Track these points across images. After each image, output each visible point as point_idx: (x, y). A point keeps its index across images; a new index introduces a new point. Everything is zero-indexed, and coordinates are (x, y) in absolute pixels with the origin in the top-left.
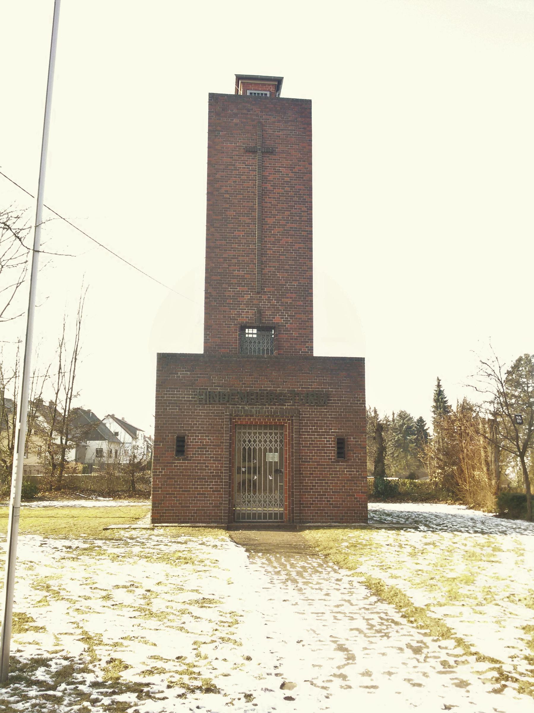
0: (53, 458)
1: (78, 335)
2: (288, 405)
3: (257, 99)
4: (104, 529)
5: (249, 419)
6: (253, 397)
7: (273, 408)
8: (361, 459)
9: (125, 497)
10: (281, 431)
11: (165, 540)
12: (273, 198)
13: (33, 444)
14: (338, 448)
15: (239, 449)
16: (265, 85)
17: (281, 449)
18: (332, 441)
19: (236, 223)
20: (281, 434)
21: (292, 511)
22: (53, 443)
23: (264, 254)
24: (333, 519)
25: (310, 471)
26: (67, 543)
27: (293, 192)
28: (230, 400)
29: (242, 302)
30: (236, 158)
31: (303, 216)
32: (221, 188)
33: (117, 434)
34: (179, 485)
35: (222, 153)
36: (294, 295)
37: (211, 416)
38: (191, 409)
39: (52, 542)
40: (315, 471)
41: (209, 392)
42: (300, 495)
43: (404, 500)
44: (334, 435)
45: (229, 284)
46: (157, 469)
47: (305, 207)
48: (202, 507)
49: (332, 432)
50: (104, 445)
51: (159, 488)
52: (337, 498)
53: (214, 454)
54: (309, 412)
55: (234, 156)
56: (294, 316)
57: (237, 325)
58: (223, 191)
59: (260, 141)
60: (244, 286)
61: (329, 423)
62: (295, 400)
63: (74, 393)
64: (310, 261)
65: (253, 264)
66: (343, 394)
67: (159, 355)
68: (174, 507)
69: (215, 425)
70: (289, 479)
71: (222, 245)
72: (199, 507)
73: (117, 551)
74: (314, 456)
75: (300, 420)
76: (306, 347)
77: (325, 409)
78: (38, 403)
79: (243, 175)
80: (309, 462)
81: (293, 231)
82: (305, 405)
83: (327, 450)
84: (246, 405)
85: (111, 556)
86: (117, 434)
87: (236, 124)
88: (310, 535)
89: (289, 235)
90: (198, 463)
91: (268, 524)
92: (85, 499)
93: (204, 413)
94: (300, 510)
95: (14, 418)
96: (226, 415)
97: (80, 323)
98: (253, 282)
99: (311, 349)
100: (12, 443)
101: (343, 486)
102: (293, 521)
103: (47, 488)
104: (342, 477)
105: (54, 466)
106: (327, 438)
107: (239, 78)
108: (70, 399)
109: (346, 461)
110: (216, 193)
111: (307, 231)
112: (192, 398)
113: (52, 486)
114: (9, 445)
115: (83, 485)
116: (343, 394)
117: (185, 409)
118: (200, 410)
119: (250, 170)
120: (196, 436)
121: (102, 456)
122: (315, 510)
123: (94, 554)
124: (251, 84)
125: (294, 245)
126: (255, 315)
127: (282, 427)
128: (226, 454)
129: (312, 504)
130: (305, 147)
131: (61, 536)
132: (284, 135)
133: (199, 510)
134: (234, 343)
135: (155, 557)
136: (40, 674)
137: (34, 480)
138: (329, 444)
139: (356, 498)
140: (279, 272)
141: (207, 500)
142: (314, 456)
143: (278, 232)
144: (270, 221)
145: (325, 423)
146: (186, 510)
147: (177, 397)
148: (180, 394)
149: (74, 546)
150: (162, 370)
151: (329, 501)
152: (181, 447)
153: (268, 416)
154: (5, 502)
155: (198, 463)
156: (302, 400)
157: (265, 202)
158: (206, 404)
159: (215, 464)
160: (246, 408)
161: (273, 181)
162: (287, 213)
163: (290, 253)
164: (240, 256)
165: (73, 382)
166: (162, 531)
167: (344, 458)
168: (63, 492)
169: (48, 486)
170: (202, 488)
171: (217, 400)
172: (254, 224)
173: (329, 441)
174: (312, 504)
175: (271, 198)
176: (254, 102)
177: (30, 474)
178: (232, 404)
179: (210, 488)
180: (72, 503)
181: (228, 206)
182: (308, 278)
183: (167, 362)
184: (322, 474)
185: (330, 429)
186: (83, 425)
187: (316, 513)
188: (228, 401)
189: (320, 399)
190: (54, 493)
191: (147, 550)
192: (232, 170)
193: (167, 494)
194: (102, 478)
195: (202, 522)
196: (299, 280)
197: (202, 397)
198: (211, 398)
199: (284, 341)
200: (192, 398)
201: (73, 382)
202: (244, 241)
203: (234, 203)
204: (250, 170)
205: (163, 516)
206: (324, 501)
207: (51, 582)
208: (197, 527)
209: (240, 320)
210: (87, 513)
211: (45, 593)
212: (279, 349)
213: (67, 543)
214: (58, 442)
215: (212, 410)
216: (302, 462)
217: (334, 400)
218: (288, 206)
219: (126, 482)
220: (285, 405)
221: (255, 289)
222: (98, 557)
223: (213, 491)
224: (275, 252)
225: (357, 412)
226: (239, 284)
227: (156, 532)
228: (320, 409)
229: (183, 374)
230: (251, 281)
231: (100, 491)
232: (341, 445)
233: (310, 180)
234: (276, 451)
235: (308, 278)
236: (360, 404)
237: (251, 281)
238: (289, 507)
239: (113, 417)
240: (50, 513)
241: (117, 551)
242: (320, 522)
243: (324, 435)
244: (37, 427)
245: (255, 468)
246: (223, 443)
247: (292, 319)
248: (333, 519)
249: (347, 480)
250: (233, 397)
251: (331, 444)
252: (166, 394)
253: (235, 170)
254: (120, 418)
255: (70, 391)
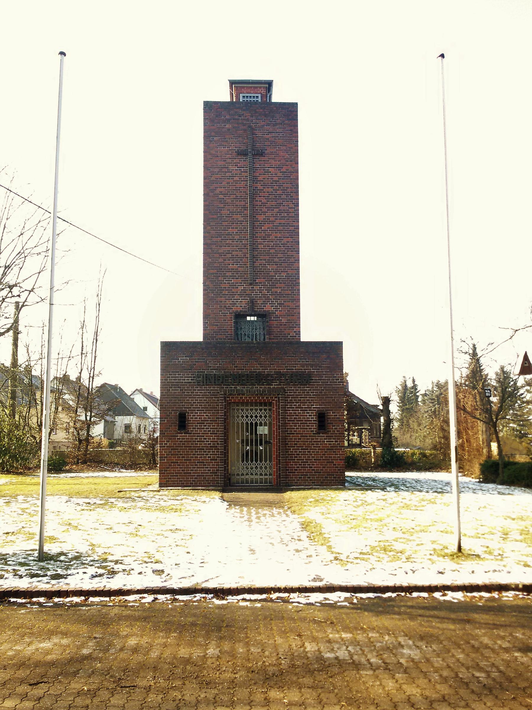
0: (78, 434)
1: (98, 317)
2: (275, 385)
3: (248, 105)
4: (118, 492)
5: (241, 398)
6: (243, 378)
7: (262, 388)
8: (339, 431)
9: (146, 469)
10: (270, 408)
11: (165, 498)
12: (263, 197)
13: (60, 420)
14: (319, 422)
15: (234, 423)
16: (256, 87)
17: (270, 423)
18: (314, 415)
19: (230, 221)
20: (270, 410)
21: (279, 476)
22: (79, 420)
23: (256, 249)
24: (315, 483)
25: (294, 441)
26: (87, 500)
27: (281, 190)
28: (224, 381)
29: (236, 292)
30: (229, 161)
31: (290, 212)
32: (216, 190)
33: (145, 409)
34: (182, 454)
35: (216, 157)
36: (283, 285)
37: (208, 395)
38: (190, 390)
39: (75, 500)
40: (298, 442)
41: (206, 374)
42: (286, 462)
43: (409, 469)
44: (315, 410)
45: (225, 277)
46: (163, 441)
47: (293, 204)
48: (202, 473)
49: (314, 408)
50: (132, 420)
51: (165, 457)
52: (318, 465)
53: (211, 428)
54: (293, 390)
55: (227, 159)
56: (283, 304)
57: (232, 313)
58: (218, 191)
59: (252, 146)
60: (238, 278)
61: (311, 400)
62: (281, 380)
63: (96, 372)
64: (297, 253)
65: (246, 258)
66: (324, 374)
67: (162, 343)
68: (178, 473)
69: (212, 403)
70: (277, 448)
71: (217, 242)
72: (199, 473)
73: (126, 505)
74: (298, 428)
75: (285, 398)
76: (294, 332)
77: (307, 387)
78: (65, 379)
79: (235, 177)
80: (294, 434)
81: (282, 226)
82: (289, 385)
83: (309, 423)
84: (238, 385)
85: (120, 508)
86: (145, 409)
87: (229, 130)
88: (288, 495)
89: (278, 230)
90: (197, 436)
91: (265, 487)
92: (109, 471)
93: (202, 393)
94: (286, 475)
95: (41, 397)
96: (221, 394)
97: (99, 305)
98: (246, 274)
99: (298, 333)
100: (41, 420)
101: (323, 454)
102: (280, 484)
103: (75, 461)
104: (322, 447)
105: (80, 441)
106: (309, 413)
107: (232, 83)
108: (93, 378)
109: (325, 433)
110: (211, 194)
111: (294, 226)
112: (191, 380)
113: (78, 460)
114: (38, 422)
115: (106, 458)
116: (324, 374)
117: (185, 390)
118: (198, 390)
119: (242, 172)
120: (195, 413)
121: (130, 432)
122: (299, 475)
123: (107, 507)
124: (244, 87)
125: (283, 240)
126: (248, 304)
127: (270, 404)
128: (221, 428)
129: (297, 470)
130: (292, 148)
131: (83, 496)
132: (272, 137)
133: (199, 476)
134: (230, 330)
135: (153, 509)
136: (62, 558)
137: (62, 454)
138: (311, 418)
139: (335, 465)
140: (269, 265)
141: (206, 468)
142: (298, 428)
143: (268, 228)
144: (261, 218)
145: (307, 400)
146: (188, 476)
147: (179, 380)
148: (181, 377)
149: (92, 503)
150: (165, 357)
151: (312, 467)
152: (182, 422)
153: (257, 395)
154: (36, 474)
155: (197, 436)
156: (287, 380)
157: (256, 201)
158: (203, 385)
159: (212, 436)
160: (238, 388)
161: (263, 181)
162: (276, 210)
163: (280, 246)
164: (234, 251)
165: (95, 362)
166: (166, 493)
167: (325, 429)
168: (89, 465)
169: (76, 460)
170: (202, 457)
171: (213, 381)
172: (246, 221)
173: (311, 416)
174: (297, 470)
175: (261, 197)
176: (244, 108)
177: (60, 449)
178: (225, 385)
179: (208, 457)
180: (96, 474)
181: (222, 206)
182: (295, 269)
183: (169, 349)
184: (305, 444)
185: (312, 405)
186: (113, 401)
187: (299, 478)
188: (222, 382)
189: (303, 379)
190: (80, 466)
191: (149, 505)
192: (226, 172)
193: (172, 463)
194: (125, 452)
195: (202, 486)
196: (287, 272)
197: (200, 379)
198: (207, 380)
199: (274, 327)
200: (191, 380)
201: (95, 362)
202: (237, 237)
203: (227, 203)
204: (242, 172)
205: (169, 481)
206: (307, 467)
207: (71, 522)
208: (196, 490)
209: (234, 309)
210: (108, 481)
211: (68, 527)
212: (270, 334)
213: (87, 500)
214: (83, 418)
215: (208, 390)
216: (288, 434)
217: (315, 380)
218: (277, 203)
219: (147, 455)
220: (272, 385)
221: (247, 281)
222: (110, 509)
223: (211, 460)
224: (265, 246)
225: (336, 390)
226: (233, 277)
227: (161, 493)
228: (303, 388)
229: (183, 359)
230: (244, 274)
231: (123, 464)
232: (322, 420)
233: (297, 179)
234: (265, 425)
235: (295, 269)
236: (339, 382)
237: (244, 274)
238: (277, 473)
239: (140, 391)
240: (76, 481)
241: (126, 505)
242: (303, 485)
243: (307, 410)
244: (65, 402)
245: (247, 440)
246: (218, 418)
247: (281, 306)
248: (315, 483)
249: (327, 449)
250: (227, 379)
251: (313, 418)
252: (169, 377)
253: (228, 172)
254: (148, 392)
255: (92, 370)
